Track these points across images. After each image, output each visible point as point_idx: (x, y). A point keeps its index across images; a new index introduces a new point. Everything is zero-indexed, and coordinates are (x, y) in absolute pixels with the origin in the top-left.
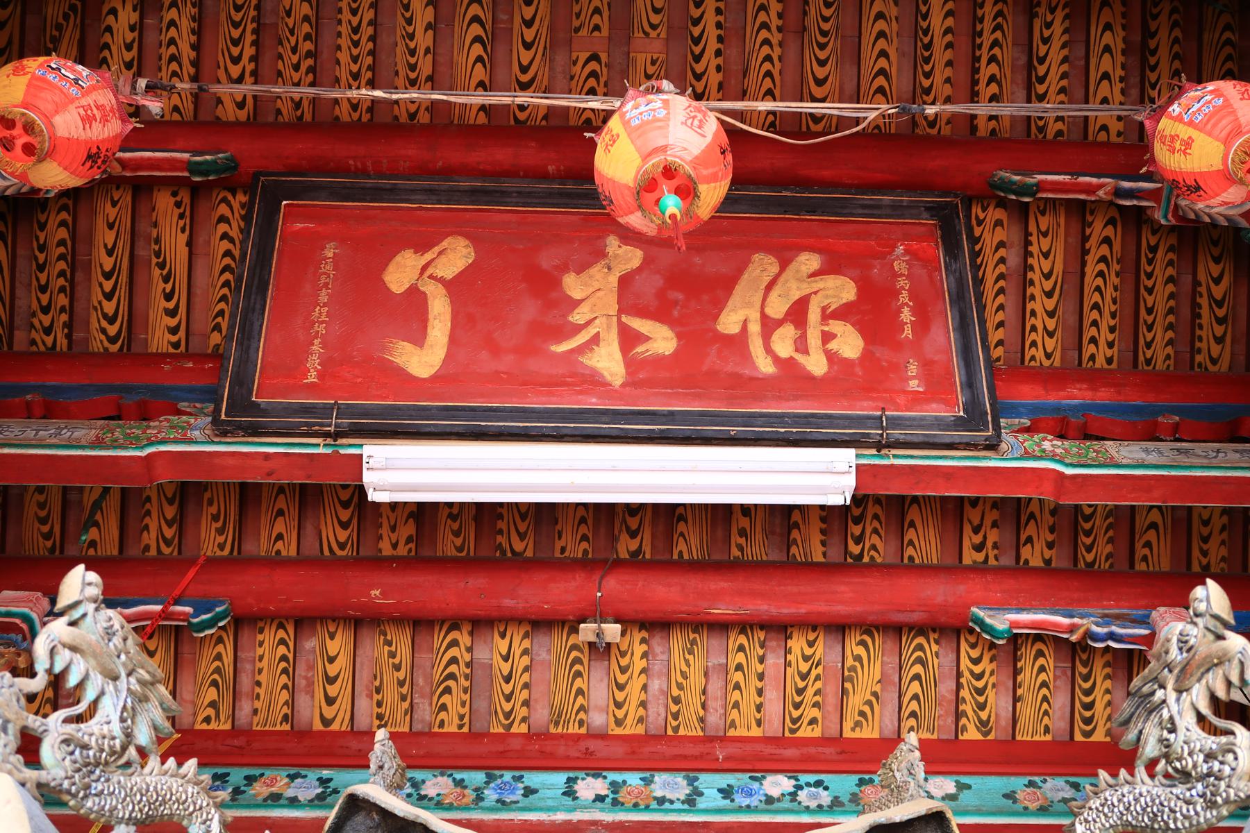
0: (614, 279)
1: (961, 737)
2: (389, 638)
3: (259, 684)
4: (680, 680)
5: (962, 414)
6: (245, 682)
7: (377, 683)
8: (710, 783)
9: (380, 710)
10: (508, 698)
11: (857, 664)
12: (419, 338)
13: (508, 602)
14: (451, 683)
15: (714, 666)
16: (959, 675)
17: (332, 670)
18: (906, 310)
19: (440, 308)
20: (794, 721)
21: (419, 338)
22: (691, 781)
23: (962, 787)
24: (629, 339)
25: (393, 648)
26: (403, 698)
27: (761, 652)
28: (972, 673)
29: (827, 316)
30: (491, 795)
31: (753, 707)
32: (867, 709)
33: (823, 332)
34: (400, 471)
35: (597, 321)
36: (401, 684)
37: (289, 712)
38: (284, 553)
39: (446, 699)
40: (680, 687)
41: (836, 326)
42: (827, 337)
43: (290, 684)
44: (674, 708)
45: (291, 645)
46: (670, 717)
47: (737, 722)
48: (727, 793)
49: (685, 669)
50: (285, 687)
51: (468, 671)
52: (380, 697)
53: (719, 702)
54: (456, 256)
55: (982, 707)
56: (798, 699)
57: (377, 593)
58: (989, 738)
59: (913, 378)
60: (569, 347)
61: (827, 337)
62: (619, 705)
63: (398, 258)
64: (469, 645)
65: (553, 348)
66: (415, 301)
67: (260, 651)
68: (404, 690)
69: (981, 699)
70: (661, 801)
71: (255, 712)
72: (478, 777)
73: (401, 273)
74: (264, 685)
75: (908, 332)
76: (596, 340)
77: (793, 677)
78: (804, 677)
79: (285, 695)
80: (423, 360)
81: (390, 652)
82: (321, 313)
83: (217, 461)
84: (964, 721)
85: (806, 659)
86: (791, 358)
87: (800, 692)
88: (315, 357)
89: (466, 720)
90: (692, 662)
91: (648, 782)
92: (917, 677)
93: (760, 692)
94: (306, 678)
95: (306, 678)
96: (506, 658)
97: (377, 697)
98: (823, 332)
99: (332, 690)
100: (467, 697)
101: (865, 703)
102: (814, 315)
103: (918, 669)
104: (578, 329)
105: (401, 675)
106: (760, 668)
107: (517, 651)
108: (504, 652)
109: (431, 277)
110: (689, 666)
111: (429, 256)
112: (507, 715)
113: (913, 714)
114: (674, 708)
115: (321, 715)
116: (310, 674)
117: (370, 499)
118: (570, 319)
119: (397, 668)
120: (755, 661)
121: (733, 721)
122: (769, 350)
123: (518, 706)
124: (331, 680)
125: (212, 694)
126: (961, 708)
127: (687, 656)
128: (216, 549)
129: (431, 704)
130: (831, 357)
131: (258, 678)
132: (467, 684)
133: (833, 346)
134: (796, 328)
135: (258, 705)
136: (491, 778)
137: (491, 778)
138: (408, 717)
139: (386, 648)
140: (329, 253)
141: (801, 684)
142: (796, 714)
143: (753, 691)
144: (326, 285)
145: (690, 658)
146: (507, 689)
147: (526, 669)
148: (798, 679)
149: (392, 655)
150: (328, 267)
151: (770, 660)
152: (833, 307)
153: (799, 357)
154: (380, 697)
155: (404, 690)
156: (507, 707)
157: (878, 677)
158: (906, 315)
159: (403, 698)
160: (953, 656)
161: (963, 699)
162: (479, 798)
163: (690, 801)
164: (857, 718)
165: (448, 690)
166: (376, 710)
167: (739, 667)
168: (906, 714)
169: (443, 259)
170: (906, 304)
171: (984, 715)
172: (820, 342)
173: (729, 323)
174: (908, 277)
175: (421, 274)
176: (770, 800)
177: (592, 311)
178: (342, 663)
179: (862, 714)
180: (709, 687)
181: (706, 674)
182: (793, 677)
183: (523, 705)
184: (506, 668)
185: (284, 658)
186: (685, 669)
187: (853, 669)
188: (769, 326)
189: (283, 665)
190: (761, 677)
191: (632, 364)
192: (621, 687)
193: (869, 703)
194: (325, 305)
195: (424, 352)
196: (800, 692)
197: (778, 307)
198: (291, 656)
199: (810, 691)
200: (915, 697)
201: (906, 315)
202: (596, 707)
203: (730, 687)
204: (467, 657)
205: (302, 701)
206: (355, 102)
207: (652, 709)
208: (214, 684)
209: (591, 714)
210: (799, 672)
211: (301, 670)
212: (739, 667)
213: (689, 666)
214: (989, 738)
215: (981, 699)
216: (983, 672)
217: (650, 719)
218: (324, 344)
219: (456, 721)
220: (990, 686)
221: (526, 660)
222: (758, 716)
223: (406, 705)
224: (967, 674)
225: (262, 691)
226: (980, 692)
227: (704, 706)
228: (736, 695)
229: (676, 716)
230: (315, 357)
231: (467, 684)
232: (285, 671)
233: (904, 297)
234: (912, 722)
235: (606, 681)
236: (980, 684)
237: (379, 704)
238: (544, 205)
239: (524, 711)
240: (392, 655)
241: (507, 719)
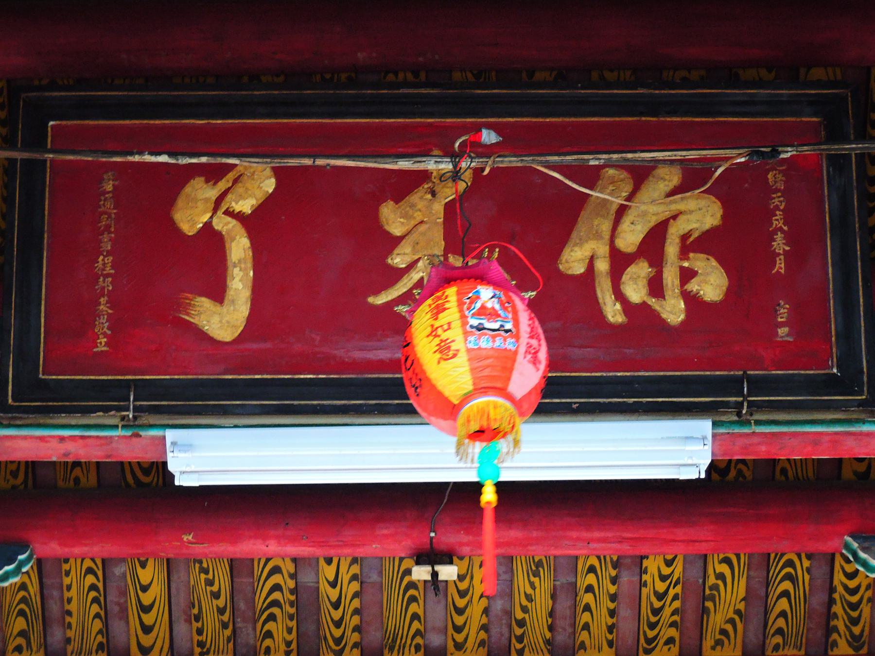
0: (438, 208)
1: (830, 653)
2: (205, 565)
3: (69, 613)
4: (525, 602)
5: (835, 371)
6: (54, 608)
7: (195, 611)
9: (200, 638)
10: (338, 624)
11: (720, 582)
12: (217, 292)
13: (340, 353)
14: (275, 610)
15: (562, 586)
16: (832, 590)
18: (779, 236)
19: (239, 248)
20: (649, 641)
21: (217, 292)
25: (210, 576)
26: (225, 626)
27: (614, 573)
28: (846, 587)
29: (688, 246)
31: (604, 627)
32: (729, 627)
33: (682, 269)
34: (206, 456)
35: (420, 264)
36: (221, 611)
37: (104, 641)
38: (83, 480)
39: (270, 626)
40: (525, 610)
41: (699, 262)
42: (687, 275)
43: (102, 613)
44: (519, 631)
45: (100, 574)
46: (514, 640)
47: (587, 643)
49: (529, 591)
50: (97, 616)
51: (293, 598)
52: (199, 625)
53: (568, 621)
55: (855, 622)
56: (653, 619)
57: (190, 537)
58: (861, 652)
59: (782, 325)
60: (390, 298)
61: (687, 275)
62: (458, 629)
63: (188, 189)
64: (292, 571)
65: (371, 300)
66: (211, 241)
67: (67, 581)
68: (225, 618)
69: (855, 614)
71: (68, 641)
74: (75, 614)
75: (780, 266)
77: (648, 597)
78: (660, 596)
79: (98, 625)
80: (224, 319)
81: (206, 580)
82: (105, 263)
83: (8, 443)
84: (835, 636)
85: (663, 578)
86: (644, 303)
87: (656, 612)
88: (103, 319)
89: (294, 646)
90: (537, 584)
92: (785, 594)
93: (612, 613)
94: (118, 604)
95: (118, 604)
96: (333, 585)
97: (196, 625)
98: (682, 269)
99: (148, 619)
100: (293, 624)
101: (727, 622)
102: (672, 249)
103: (787, 585)
104: (399, 274)
105: (221, 602)
106: (613, 589)
107: (345, 577)
108: (331, 579)
109: (228, 213)
110: (534, 589)
111: (223, 185)
112: (338, 641)
113: (780, 631)
114: (519, 631)
115: (139, 644)
116: (122, 601)
117: (177, 483)
118: (389, 261)
119: (216, 595)
120: (607, 583)
121: (583, 643)
122: (619, 296)
123: (348, 632)
124: (147, 609)
125: (20, 624)
126: (832, 623)
127: (532, 579)
128: (9, 476)
129: (255, 629)
130: (692, 301)
131: (67, 607)
132: (292, 611)
133: (693, 286)
134: (651, 266)
135: (70, 634)
138: (231, 645)
139: (203, 576)
140: (109, 187)
141: (657, 604)
142: (651, 634)
143: (605, 612)
144: (108, 227)
145: (536, 580)
146: (337, 615)
147: (356, 595)
148: (653, 599)
149: (210, 583)
150: (108, 205)
151: (625, 578)
152: (696, 235)
153: (652, 302)
154: (199, 625)
155: (225, 618)
156: (337, 633)
157: (742, 593)
158: (779, 244)
159: (225, 626)
160: (826, 569)
161: (835, 614)
164: (718, 637)
165: (272, 618)
166: (196, 638)
167: (589, 589)
168: (772, 632)
169: (239, 189)
170: (781, 229)
171: (856, 630)
172: (677, 282)
173: (573, 261)
174: (784, 193)
175: (215, 210)
177: (414, 251)
178: (156, 592)
179: (723, 632)
180: (558, 607)
181: (553, 597)
182: (648, 597)
183: (354, 630)
184: (334, 594)
185: (93, 587)
186: (529, 591)
187: (715, 587)
188: (620, 262)
189: (93, 594)
190: (613, 598)
192: (460, 612)
193: (732, 621)
194: (109, 253)
195: (224, 309)
196: (656, 612)
197: (630, 237)
198: (100, 585)
199: (667, 611)
200: (783, 614)
201: (779, 244)
202: (434, 628)
203: (580, 609)
204: (291, 584)
205: (117, 626)
206: (146, 466)
207: (494, 630)
208: (22, 613)
209: (427, 636)
210: (656, 593)
211: (112, 597)
212: (589, 589)
213: (534, 589)
214: (861, 652)
215: (855, 614)
216: (858, 587)
217: (493, 640)
218: (112, 304)
219: (283, 647)
220: (865, 601)
221: (355, 586)
222: (610, 637)
223: (228, 632)
224: (840, 589)
225: (73, 620)
226: (854, 607)
227: (551, 628)
228: (586, 617)
229: (520, 639)
230: (103, 319)
231: (292, 611)
232: (95, 600)
233: (778, 221)
234: (778, 639)
235: (443, 602)
236: (854, 599)
237: (200, 632)
239: (356, 637)
240: (210, 583)
241: (337, 644)
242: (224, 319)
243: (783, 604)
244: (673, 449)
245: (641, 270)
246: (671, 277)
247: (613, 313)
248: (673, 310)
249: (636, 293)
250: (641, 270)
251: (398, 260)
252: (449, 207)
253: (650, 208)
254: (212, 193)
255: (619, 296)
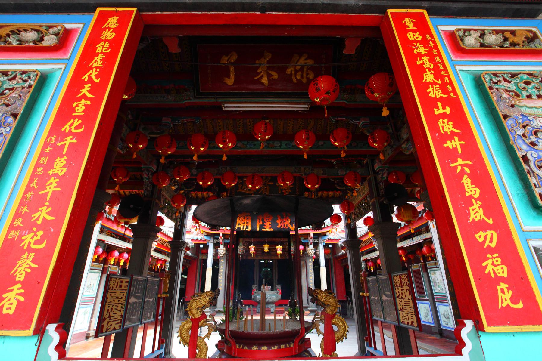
8: (284, 143)
12: (229, 77)
17: (220, 124)
21: (229, 77)
22: (281, 143)
23: (324, 143)
24: (269, 76)
30: (248, 146)
41: (310, 72)
42: (307, 74)
48: (286, 145)
54: (234, 58)
61: (307, 74)
70: (276, 146)
72: (246, 142)
73: (224, 60)
76: (262, 76)
80: (230, 82)
91: (273, 143)
102: (305, 70)
111: (228, 57)
122: (296, 78)
136: (248, 143)
137: (248, 143)
162: (247, 146)
163: (280, 147)
176: (293, 146)
191: (269, 80)
197: (298, 68)
238: (258, 103)
242: (230, 82)
243: (320, 126)
244: (164, 345)
245: (299, 73)
246: (305, 75)
247: (295, 81)
248: (304, 80)
249: (298, 77)
250: (299, 73)
251: (259, 71)
252: (290, 306)
253: (302, 61)
254: (227, 58)
255: (296, 78)
